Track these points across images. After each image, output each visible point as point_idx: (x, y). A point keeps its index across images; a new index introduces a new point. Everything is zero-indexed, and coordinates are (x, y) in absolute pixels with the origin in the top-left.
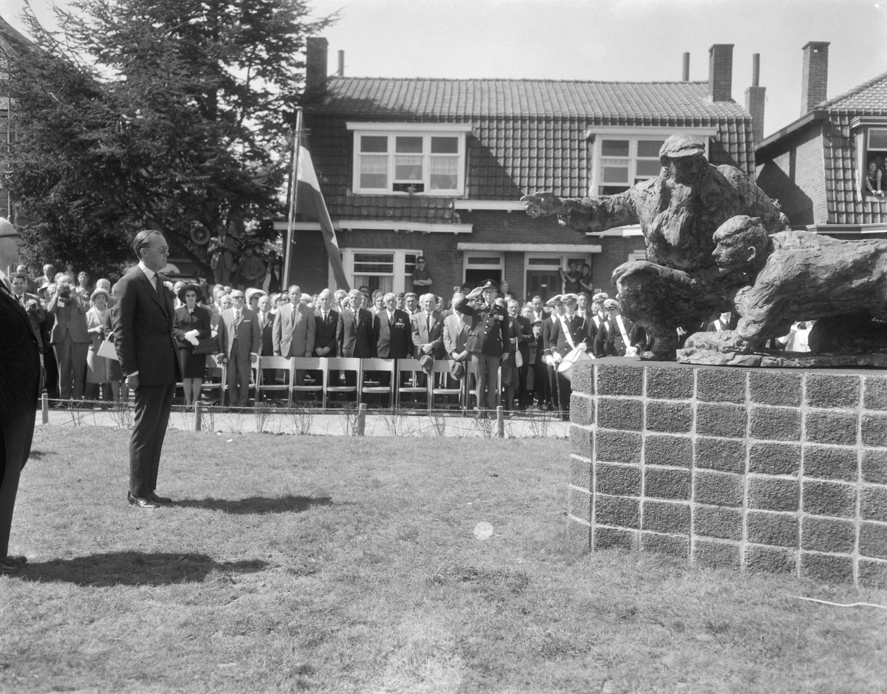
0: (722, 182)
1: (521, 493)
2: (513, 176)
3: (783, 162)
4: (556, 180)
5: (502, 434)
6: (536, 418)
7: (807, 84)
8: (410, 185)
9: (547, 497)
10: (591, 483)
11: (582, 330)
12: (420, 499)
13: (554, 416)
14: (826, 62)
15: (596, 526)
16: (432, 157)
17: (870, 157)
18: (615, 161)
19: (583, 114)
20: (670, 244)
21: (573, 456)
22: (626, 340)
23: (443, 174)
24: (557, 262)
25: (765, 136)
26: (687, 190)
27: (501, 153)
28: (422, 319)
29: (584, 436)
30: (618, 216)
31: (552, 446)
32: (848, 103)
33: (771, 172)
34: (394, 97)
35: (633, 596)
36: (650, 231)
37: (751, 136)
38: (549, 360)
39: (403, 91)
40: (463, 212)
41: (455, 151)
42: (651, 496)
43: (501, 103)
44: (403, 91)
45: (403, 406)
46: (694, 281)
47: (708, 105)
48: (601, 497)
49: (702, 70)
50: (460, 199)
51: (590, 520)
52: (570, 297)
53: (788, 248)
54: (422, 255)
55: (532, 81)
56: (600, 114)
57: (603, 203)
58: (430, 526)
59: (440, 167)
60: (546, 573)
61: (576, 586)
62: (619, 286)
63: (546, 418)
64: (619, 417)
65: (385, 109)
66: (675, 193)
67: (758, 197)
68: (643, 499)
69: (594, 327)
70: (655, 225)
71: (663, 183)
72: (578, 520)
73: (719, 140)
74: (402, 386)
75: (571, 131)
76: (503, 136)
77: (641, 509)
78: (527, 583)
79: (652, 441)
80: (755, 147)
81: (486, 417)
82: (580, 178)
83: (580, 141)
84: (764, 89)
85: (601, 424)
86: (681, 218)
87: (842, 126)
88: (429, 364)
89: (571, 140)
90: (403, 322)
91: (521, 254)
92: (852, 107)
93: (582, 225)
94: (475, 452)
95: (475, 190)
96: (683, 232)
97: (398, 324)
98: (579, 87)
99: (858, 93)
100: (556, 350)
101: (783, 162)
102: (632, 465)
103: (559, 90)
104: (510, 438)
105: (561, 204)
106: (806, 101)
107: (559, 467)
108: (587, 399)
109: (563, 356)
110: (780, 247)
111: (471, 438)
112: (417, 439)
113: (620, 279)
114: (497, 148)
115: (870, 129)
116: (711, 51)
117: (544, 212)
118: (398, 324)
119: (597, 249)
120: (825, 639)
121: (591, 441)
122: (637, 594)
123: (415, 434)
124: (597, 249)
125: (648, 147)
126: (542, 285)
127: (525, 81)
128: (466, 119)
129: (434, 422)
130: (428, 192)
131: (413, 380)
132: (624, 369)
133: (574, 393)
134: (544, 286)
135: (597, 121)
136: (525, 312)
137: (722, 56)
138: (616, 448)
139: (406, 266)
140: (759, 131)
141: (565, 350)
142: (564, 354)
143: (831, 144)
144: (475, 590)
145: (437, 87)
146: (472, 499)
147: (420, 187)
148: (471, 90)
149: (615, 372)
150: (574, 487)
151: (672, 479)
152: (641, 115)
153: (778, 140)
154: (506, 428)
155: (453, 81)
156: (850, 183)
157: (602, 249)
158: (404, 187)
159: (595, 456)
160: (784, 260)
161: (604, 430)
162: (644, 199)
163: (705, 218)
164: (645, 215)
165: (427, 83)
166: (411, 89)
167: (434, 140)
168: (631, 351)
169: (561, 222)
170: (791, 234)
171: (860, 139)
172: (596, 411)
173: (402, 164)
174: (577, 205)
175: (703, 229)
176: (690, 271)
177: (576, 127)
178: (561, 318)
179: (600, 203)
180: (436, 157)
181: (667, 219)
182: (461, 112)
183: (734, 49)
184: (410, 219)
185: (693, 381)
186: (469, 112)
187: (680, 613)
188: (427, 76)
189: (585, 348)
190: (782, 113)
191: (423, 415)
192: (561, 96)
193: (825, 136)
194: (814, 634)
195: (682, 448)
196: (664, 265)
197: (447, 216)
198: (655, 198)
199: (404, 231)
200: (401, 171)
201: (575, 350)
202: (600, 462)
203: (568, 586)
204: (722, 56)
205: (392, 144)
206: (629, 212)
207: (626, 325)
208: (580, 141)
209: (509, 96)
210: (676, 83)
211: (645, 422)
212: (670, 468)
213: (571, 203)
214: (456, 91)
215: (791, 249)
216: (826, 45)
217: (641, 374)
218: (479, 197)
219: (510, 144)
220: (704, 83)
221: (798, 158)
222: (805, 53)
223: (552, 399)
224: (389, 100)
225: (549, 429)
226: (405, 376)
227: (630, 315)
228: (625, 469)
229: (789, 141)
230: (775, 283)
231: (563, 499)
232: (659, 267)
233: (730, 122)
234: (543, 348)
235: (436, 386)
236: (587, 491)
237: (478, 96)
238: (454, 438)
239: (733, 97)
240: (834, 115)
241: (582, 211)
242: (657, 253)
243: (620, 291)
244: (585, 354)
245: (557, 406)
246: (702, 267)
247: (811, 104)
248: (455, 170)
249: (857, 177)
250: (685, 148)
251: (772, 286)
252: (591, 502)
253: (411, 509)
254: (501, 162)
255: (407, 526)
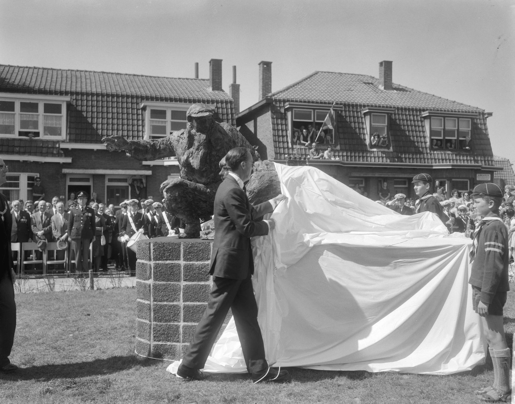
0: (223, 132)
1: (106, 325)
2: (97, 129)
3: (250, 125)
4: (124, 132)
5: (92, 287)
6: (114, 276)
7: (261, 84)
8: (30, 132)
9: (122, 326)
10: (150, 317)
11: (140, 221)
12: (37, 335)
13: (126, 274)
14: (270, 72)
15: (153, 343)
16: (45, 116)
17: (294, 124)
18: (158, 122)
19: (139, 94)
20: (194, 168)
21: (139, 300)
22: (169, 226)
23: (52, 126)
24: (125, 180)
25: (241, 110)
26: (203, 137)
27: (89, 115)
28: (37, 216)
29: (145, 287)
30: (163, 151)
31: (125, 293)
32: (282, 95)
33: (245, 131)
34: (19, 77)
35: (178, 386)
36: (182, 161)
37: (234, 110)
38: (123, 239)
39: (25, 74)
40: (66, 150)
41: (60, 112)
42: (187, 321)
43: (89, 85)
44: (25, 74)
45: (26, 273)
46: (208, 190)
47: (209, 92)
48: (157, 325)
49: (205, 73)
50: (63, 142)
51: (150, 340)
52: (133, 201)
53: (261, 171)
54: (38, 176)
55: (107, 73)
56: (149, 94)
57: (154, 144)
58: (43, 353)
59: (50, 122)
60: (123, 377)
61: (142, 384)
62: (165, 193)
63: (121, 275)
64: (166, 274)
65: (13, 84)
66: (196, 138)
67: (243, 141)
68: (182, 324)
69: (148, 219)
70: (185, 157)
71: (189, 132)
72: (142, 340)
73: (216, 112)
74: (26, 260)
75: (132, 103)
76: (90, 104)
77: (181, 330)
78: (110, 386)
79: (187, 288)
80: (236, 117)
81: (83, 277)
82: (138, 131)
83: (137, 110)
84: (239, 85)
85: (156, 279)
86: (200, 153)
87: (280, 107)
88: (44, 246)
89: (132, 109)
90: (26, 219)
91: (103, 176)
92: (284, 97)
93: (141, 157)
94: (75, 300)
95: (73, 137)
96: (201, 161)
97: (22, 220)
98: (136, 78)
99: (287, 90)
100: (126, 233)
101: (250, 125)
102: (175, 303)
103: (124, 79)
104: (98, 289)
105: (127, 143)
106: (261, 93)
107: (129, 306)
108: (147, 264)
109: (130, 237)
110: (256, 170)
111: (72, 291)
112: (36, 294)
113: (165, 189)
114: (87, 112)
115: (294, 109)
116: (210, 62)
117: (117, 148)
118: (22, 220)
119: (149, 173)
120: (290, 399)
121: (150, 290)
122: (180, 384)
123: (35, 291)
124: (149, 173)
125: (176, 114)
126: (115, 195)
127: (103, 73)
128: (66, 93)
129: (47, 282)
130: (43, 137)
131: (33, 256)
132: (169, 244)
133: (138, 261)
134: (118, 195)
135: (147, 98)
136: (107, 211)
137: (216, 66)
138: (163, 293)
139: (28, 183)
140: (237, 108)
141: (131, 233)
142: (131, 236)
143: (275, 117)
144: (75, 395)
145: (48, 73)
146: (73, 332)
147: (37, 134)
148: (69, 76)
149: (164, 246)
150: (139, 319)
151: (199, 311)
152: (172, 96)
153: (248, 113)
154: (95, 283)
155: (58, 70)
156: (285, 138)
157: (152, 173)
158: (26, 134)
159: (152, 299)
160: (259, 178)
161: (157, 282)
162: (178, 141)
163: (214, 153)
164: (179, 151)
165: (41, 71)
166: (30, 73)
167: (46, 105)
168: (172, 233)
169: (128, 154)
170: (262, 163)
171: (289, 114)
172: (152, 271)
173: (25, 119)
174: (138, 144)
175: (213, 159)
176: (206, 184)
177: (135, 101)
178: (129, 213)
179: (152, 143)
180: (47, 116)
181: (192, 153)
182: (63, 89)
183: (223, 63)
184: (30, 154)
185: (210, 250)
186: (68, 89)
187: (207, 394)
188: (41, 66)
189: (143, 232)
190: (249, 99)
191: (40, 278)
192: (125, 83)
193: (272, 112)
194: (284, 397)
195: (205, 291)
196: (191, 181)
197: (55, 152)
198: (185, 141)
199: (27, 161)
200: (24, 124)
201: (137, 233)
202: (155, 303)
203: (137, 384)
204: (216, 66)
205: (17, 107)
206: (169, 149)
207: (168, 217)
208: (137, 110)
209: (93, 81)
210: (191, 79)
211: (182, 276)
212: (198, 303)
213: (133, 143)
214: (60, 76)
215: (262, 171)
216: (271, 63)
217: (180, 247)
218: (76, 141)
219: (95, 109)
220: (207, 80)
221: (258, 124)
222: (260, 67)
223: (124, 263)
224: (16, 79)
225: (122, 282)
226: (28, 253)
227: (172, 211)
228: (171, 306)
229: (254, 114)
230: (255, 191)
231: (132, 327)
232: (188, 182)
233: (222, 102)
234: (119, 232)
235: (49, 259)
236: (148, 322)
237: (74, 80)
238: (61, 292)
239: (223, 88)
240: (276, 101)
241: (141, 148)
242: (187, 174)
243: (165, 197)
244: (143, 236)
245: (127, 267)
246: (213, 182)
247: (264, 94)
248: (60, 124)
249: (288, 135)
250: (202, 112)
251: (253, 192)
252: (150, 328)
253: (30, 343)
254: (90, 120)
255: (27, 355)
